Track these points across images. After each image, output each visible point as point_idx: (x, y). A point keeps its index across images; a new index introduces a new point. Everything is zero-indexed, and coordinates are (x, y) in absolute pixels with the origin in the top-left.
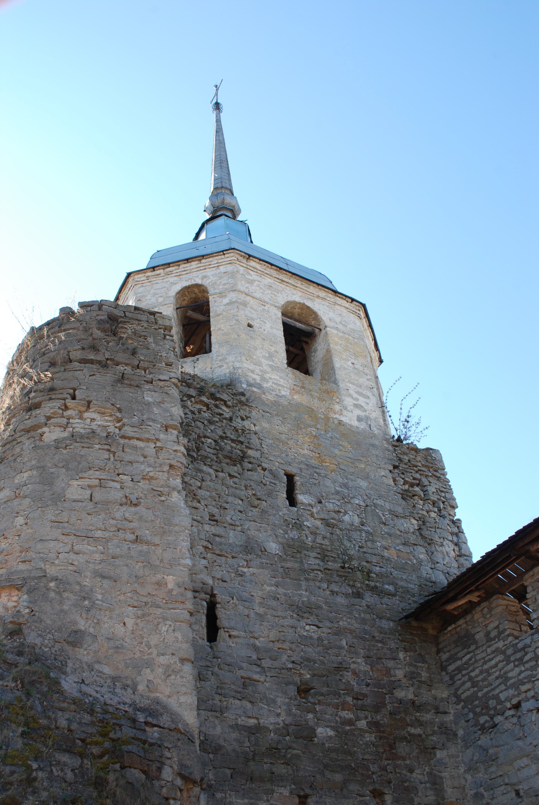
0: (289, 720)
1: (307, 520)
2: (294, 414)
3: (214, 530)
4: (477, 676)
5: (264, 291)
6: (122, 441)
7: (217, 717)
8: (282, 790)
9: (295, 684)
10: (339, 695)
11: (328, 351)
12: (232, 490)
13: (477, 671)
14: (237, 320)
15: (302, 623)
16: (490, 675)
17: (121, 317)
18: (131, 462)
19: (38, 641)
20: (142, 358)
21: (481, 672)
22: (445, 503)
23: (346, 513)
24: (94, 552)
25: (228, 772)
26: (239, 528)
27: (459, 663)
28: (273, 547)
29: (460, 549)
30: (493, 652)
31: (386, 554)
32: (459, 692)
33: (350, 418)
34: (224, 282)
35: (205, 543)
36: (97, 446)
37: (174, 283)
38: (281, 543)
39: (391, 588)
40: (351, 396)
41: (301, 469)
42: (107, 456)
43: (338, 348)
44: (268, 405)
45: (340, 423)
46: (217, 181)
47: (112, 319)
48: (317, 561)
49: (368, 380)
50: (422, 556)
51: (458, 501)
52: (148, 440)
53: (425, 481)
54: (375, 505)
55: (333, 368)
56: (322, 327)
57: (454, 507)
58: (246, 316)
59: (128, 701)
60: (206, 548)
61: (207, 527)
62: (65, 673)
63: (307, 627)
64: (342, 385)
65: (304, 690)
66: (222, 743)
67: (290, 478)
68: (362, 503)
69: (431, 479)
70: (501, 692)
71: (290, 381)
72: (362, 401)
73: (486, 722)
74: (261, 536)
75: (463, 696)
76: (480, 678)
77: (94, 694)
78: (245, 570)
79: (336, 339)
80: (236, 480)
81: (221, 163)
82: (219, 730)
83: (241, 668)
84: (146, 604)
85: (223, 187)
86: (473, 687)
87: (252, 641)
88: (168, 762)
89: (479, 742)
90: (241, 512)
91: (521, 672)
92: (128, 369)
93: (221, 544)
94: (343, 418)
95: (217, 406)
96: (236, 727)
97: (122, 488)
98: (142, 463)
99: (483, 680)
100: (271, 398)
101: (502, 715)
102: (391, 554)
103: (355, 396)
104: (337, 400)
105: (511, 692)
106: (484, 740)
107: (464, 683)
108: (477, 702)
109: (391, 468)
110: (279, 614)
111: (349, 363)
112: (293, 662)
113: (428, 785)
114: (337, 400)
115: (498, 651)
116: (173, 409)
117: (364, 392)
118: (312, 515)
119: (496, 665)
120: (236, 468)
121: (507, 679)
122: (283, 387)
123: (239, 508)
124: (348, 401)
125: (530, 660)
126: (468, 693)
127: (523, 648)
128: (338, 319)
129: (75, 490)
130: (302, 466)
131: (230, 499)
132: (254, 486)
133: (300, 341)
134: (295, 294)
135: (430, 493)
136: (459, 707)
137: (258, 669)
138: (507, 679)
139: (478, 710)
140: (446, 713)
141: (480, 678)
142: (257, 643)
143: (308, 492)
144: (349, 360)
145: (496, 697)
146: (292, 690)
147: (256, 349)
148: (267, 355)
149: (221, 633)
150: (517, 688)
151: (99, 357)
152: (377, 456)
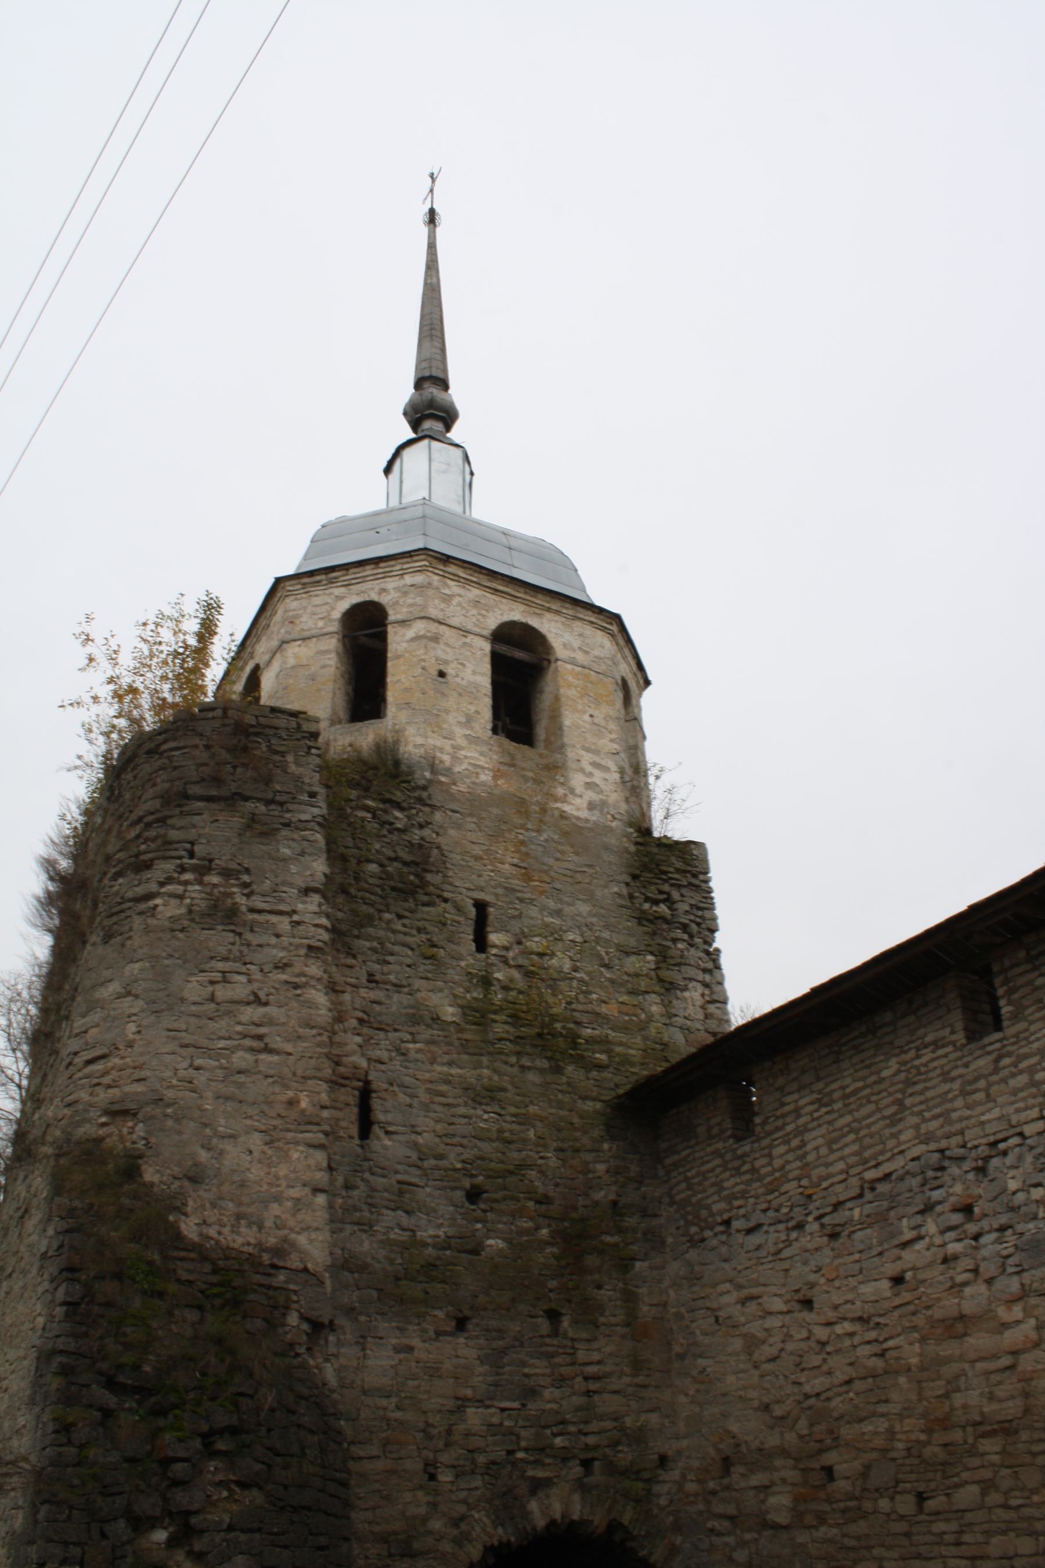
0: (451, 1231)
1: (499, 971)
2: (495, 811)
3: (372, 995)
4: (693, 1177)
5: (468, 611)
6: (251, 916)
7: (365, 1231)
8: (437, 1312)
9: (462, 1188)
10: (518, 1200)
11: (557, 699)
12: (401, 937)
13: (694, 1172)
14: (423, 668)
15: (479, 1112)
16: (706, 1179)
17: (252, 726)
18: (260, 946)
19: (156, 1179)
20: (278, 788)
21: (698, 1174)
22: (702, 924)
23: (553, 955)
24: (216, 1068)
25: (374, 1294)
26: (406, 990)
27: (676, 1157)
28: (449, 1012)
29: (712, 993)
30: (712, 1153)
31: (604, 1009)
32: (674, 1192)
33: (577, 807)
34: (410, 601)
35: (360, 1015)
36: (220, 927)
37: (342, 600)
38: (462, 1007)
39: (603, 1057)
40: (582, 770)
41: (496, 895)
42: (232, 940)
43: (572, 693)
44: (458, 801)
45: (563, 816)
46: (424, 365)
47: (241, 730)
48: (507, 1027)
49: (612, 741)
50: (654, 1009)
51: (720, 922)
52: (281, 913)
53: (675, 895)
54: (598, 940)
55: (560, 728)
56: (552, 659)
57: (713, 930)
58: (437, 659)
59: (252, 1241)
60: (361, 1021)
61: (363, 992)
62: (186, 1215)
63: (486, 1116)
64: (571, 754)
65: (474, 1195)
66: (369, 1260)
67: (481, 907)
68: (579, 939)
69: (684, 891)
70: (714, 1202)
71: (495, 757)
72: (598, 777)
73: (696, 1233)
74: (435, 999)
75: (678, 1198)
76: (696, 1181)
77: (216, 1235)
78: (411, 1046)
79: (570, 678)
80: (406, 921)
81: (432, 328)
82: (366, 1246)
83: (397, 1172)
84: (275, 1127)
85: (431, 378)
86: (688, 1189)
87: (413, 1137)
88: (295, 1306)
89: (687, 1256)
90: (409, 966)
91: (737, 1184)
92: (262, 808)
93: (380, 1014)
94: (566, 808)
95: (385, 811)
96: (387, 1243)
97: (250, 981)
98: (274, 947)
99: (700, 1184)
100: (462, 788)
101: (712, 1229)
102: (609, 1009)
103: (589, 768)
104: (562, 780)
105: (722, 1205)
106: (692, 1255)
107: (679, 1183)
108: (689, 1209)
109: (628, 879)
110: (450, 1101)
111: (587, 717)
112: (463, 1161)
113: (618, 1303)
114: (562, 780)
115: (717, 1153)
116: (315, 864)
117: (603, 763)
118: (505, 962)
119: (712, 1170)
120: (406, 905)
121: (722, 1189)
122: (483, 768)
123: (408, 961)
124: (577, 781)
125: (747, 1172)
126: (682, 1196)
127: (742, 1157)
128: (576, 643)
129: (194, 989)
130: (500, 891)
131: (396, 948)
132: (430, 928)
133: (519, 675)
134: (515, 613)
135: (681, 911)
136: (671, 1209)
137: (419, 1172)
138: (722, 1189)
139: (690, 1218)
140: (655, 1216)
141: (696, 1181)
142: (420, 1140)
143: (503, 929)
144: (584, 712)
145: (708, 1207)
146: (459, 1195)
147: (447, 711)
148: (463, 720)
149: (376, 1129)
150: (730, 1203)
151: (224, 792)
152: (610, 863)
